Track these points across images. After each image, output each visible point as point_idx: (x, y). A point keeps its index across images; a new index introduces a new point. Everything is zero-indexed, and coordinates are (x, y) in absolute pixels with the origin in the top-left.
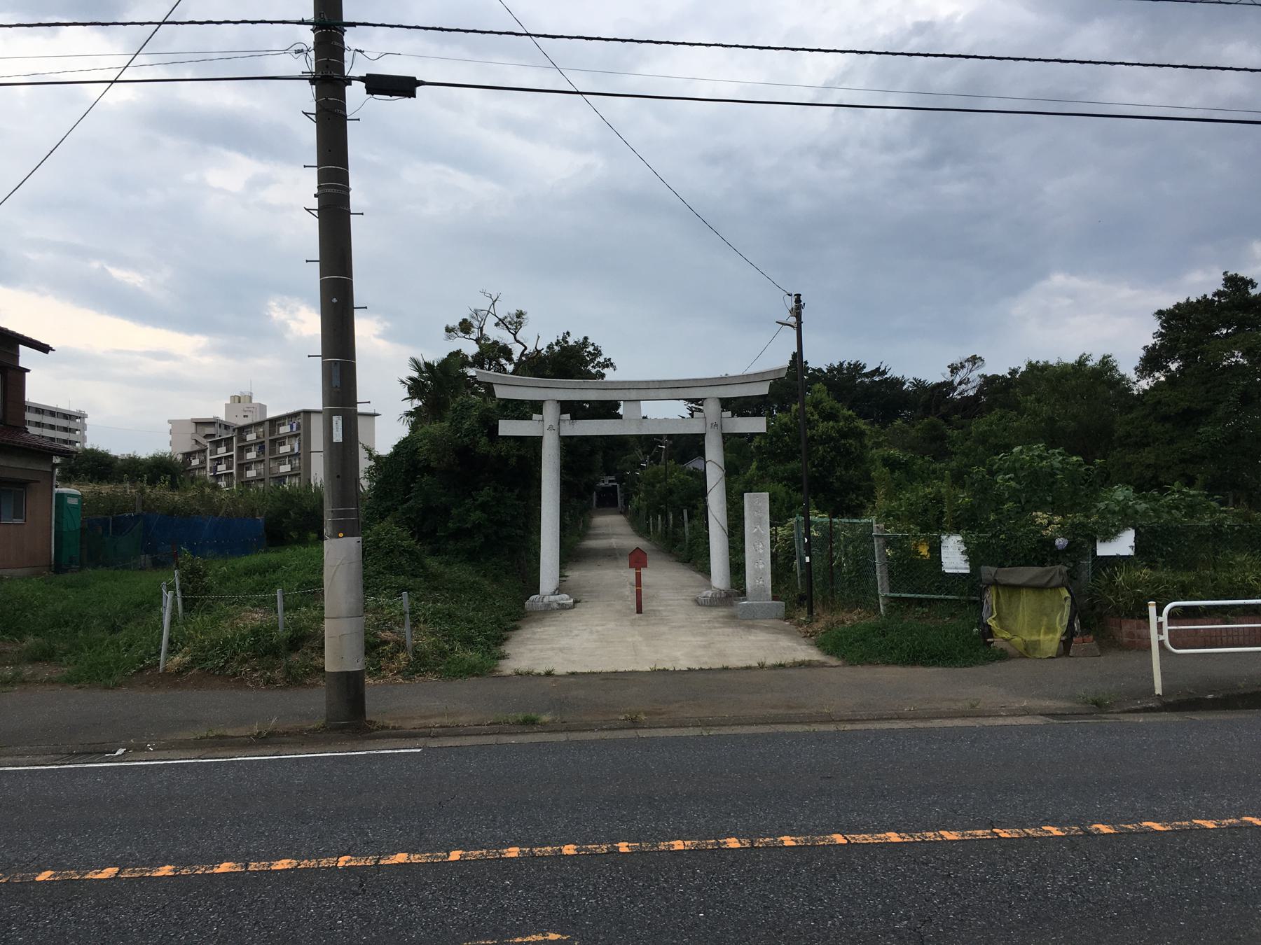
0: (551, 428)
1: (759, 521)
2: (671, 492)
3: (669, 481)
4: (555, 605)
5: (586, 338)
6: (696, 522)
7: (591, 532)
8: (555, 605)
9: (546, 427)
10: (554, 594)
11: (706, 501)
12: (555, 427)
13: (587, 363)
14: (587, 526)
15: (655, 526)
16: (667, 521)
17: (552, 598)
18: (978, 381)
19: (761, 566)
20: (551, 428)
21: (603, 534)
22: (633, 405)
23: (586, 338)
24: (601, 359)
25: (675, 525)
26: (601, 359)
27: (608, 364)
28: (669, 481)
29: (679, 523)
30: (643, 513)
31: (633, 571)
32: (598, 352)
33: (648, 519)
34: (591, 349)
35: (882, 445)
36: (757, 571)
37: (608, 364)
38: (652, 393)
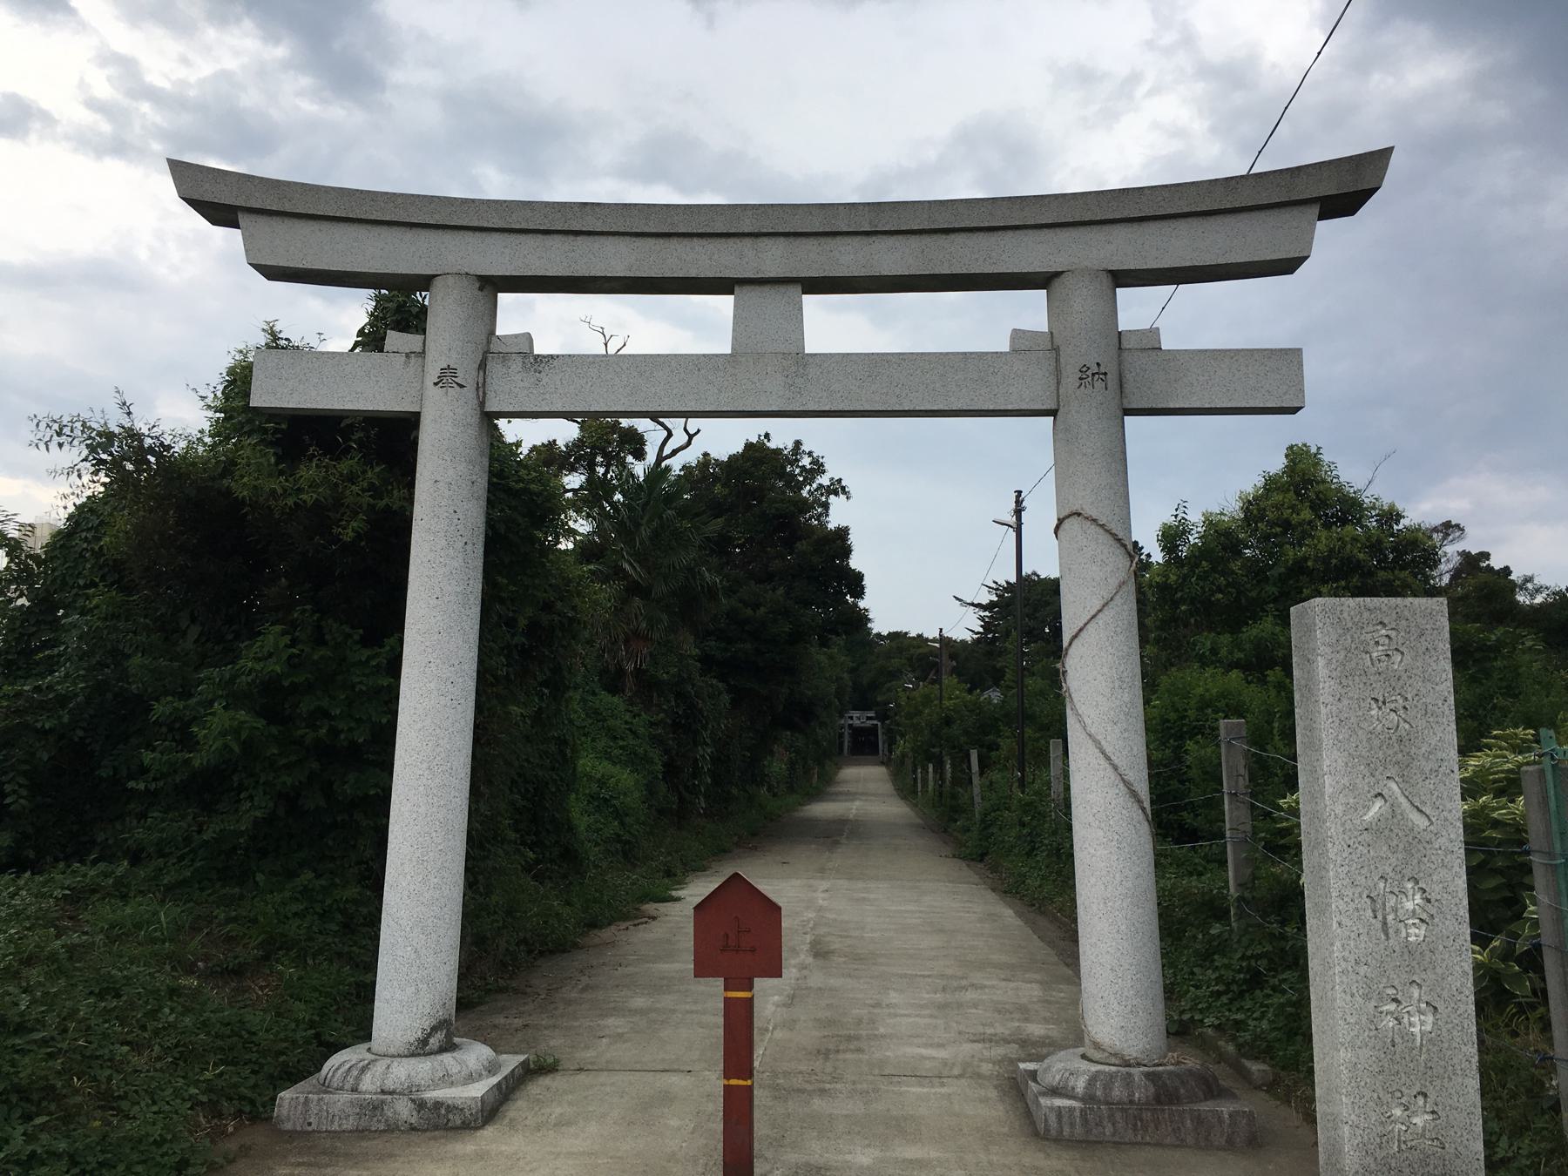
0: (447, 377)
1: (1394, 756)
2: (948, 722)
3: (946, 703)
4: (403, 1110)
5: (798, 443)
6: (995, 776)
7: (833, 789)
8: (403, 1110)
9: (433, 374)
10: (421, 1048)
11: (1055, 679)
12: (466, 374)
13: (800, 486)
14: (828, 779)
15: (925, 781)
16: (942, 779)
17: (423, 1068)
18: (1456, 560)
19: (1421, 1024)
20: (447, 377)
21: (848, 793)
22: (770, 299)
23: (798, 443)
24: (824, 480)
25: (956, 781)
26: (824, 480)
27: (837, 488)
28: (946, 703)
29: (963, 780)
30: (909, 762)
31: (714, 988)
32: (818, 468)
33: (915, 772)
34: (806, 461)
35: (1274, 675)
36: (1396, 1060)
37: (837, 488)
38: (848, 258)
